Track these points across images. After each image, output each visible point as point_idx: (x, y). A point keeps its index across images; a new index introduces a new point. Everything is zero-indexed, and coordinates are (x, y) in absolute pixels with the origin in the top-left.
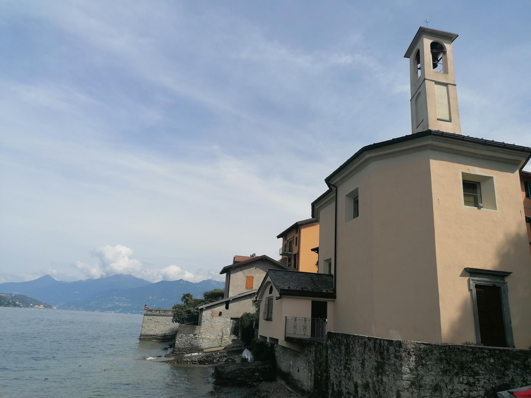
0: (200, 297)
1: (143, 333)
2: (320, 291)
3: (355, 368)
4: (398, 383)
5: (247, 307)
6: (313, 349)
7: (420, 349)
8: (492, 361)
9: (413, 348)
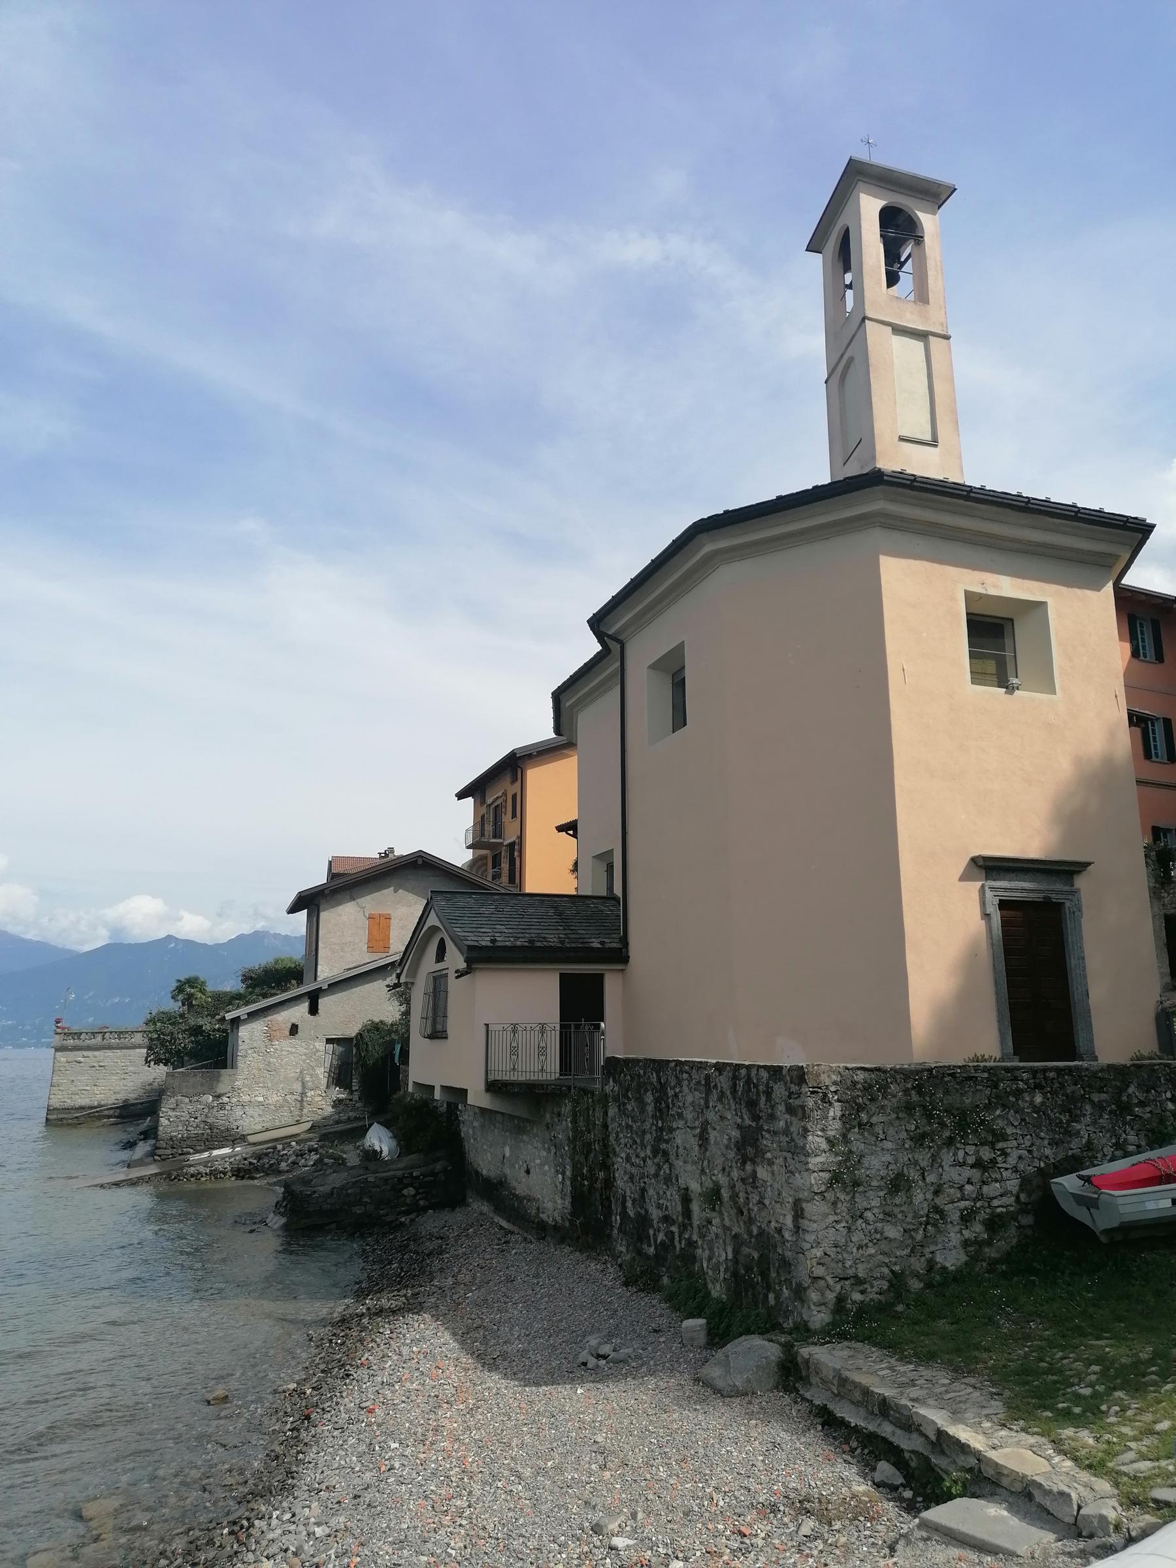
0: (233, 985)
1: (56, 1102)
2: (582, 945)
3: (681, 1151)
4: (798, 1180)
5: (375, 1005)
6: (567, 1108)
7: (855, 1083)
8: (1038, 1099)
9: (835, 1083)
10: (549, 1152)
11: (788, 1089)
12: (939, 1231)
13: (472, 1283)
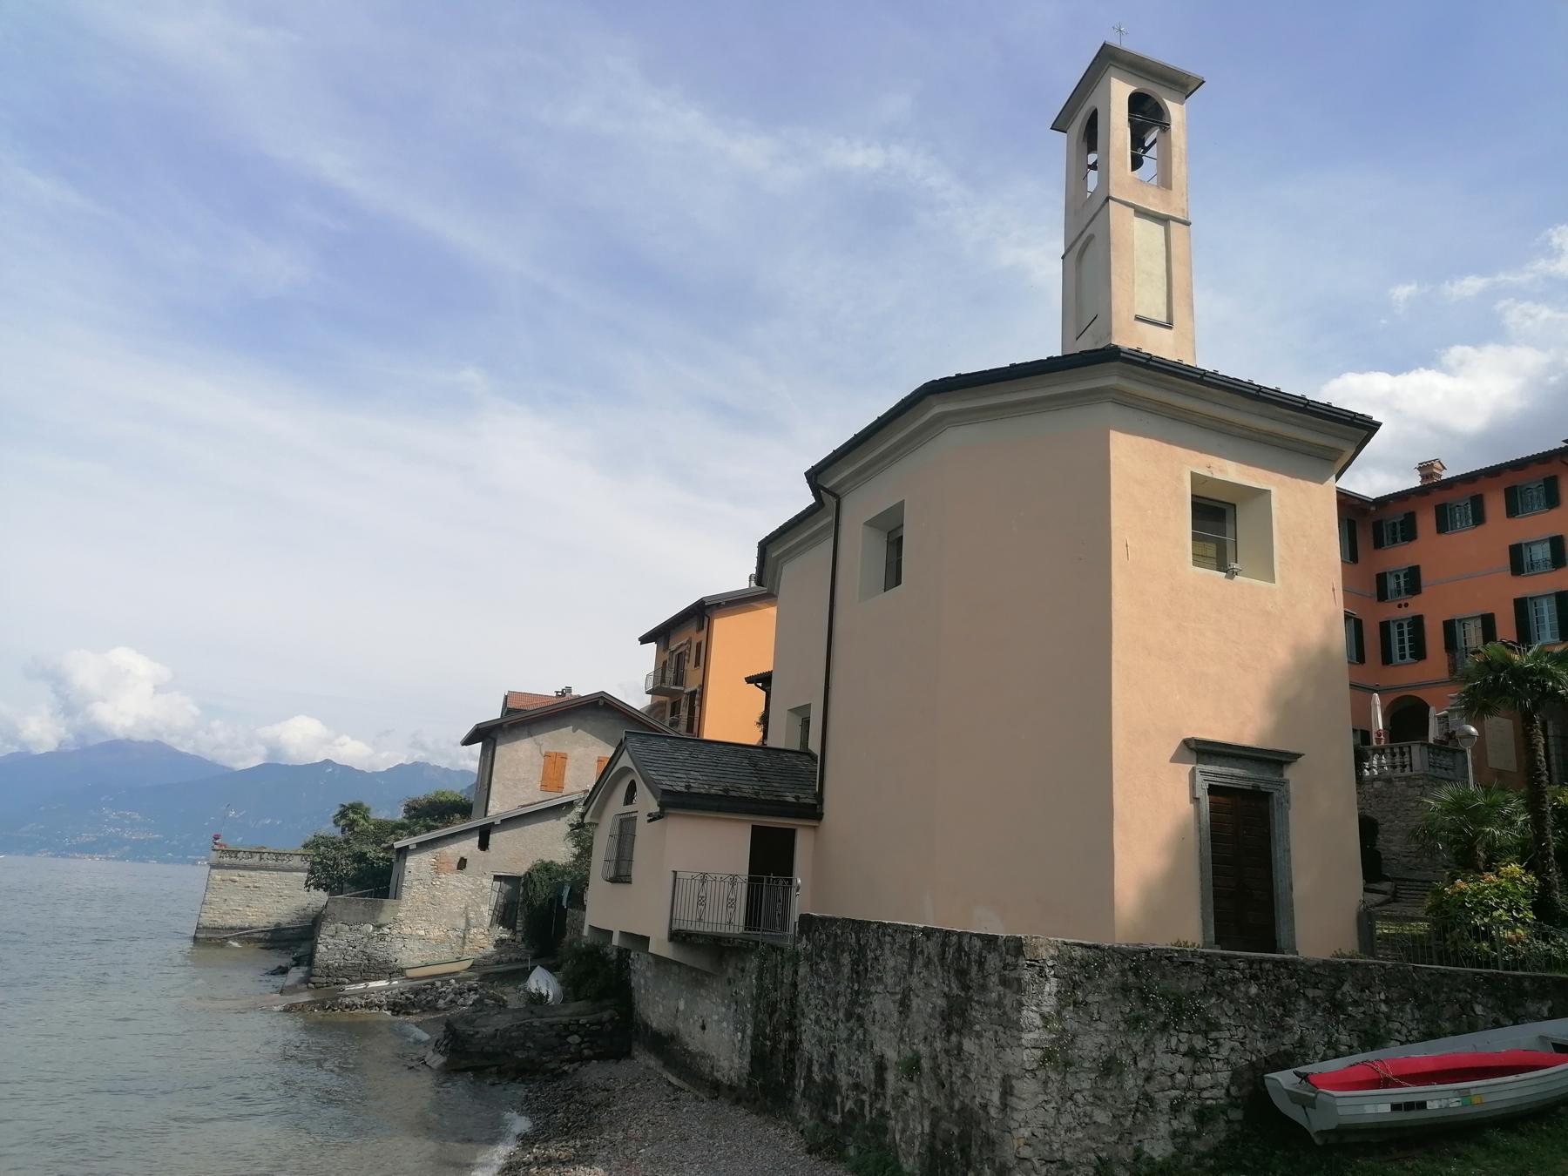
0: (399, 816)
1: (206, 920)
2: (775, 797)
3: (878, 1017)
4: (1008, 1056)
5: (551, 844)
6: (753, 963)
7: (1072, 959)
8: (1253, 990)
9: (1052, 958)
10: (729, 1007)
11: (1003, 960)
12: (1147, 1119)
13: (644, 1139)
